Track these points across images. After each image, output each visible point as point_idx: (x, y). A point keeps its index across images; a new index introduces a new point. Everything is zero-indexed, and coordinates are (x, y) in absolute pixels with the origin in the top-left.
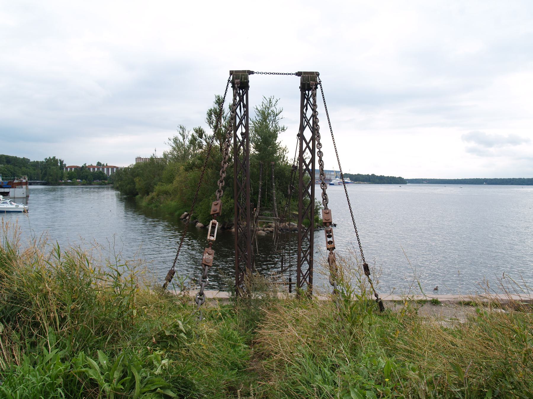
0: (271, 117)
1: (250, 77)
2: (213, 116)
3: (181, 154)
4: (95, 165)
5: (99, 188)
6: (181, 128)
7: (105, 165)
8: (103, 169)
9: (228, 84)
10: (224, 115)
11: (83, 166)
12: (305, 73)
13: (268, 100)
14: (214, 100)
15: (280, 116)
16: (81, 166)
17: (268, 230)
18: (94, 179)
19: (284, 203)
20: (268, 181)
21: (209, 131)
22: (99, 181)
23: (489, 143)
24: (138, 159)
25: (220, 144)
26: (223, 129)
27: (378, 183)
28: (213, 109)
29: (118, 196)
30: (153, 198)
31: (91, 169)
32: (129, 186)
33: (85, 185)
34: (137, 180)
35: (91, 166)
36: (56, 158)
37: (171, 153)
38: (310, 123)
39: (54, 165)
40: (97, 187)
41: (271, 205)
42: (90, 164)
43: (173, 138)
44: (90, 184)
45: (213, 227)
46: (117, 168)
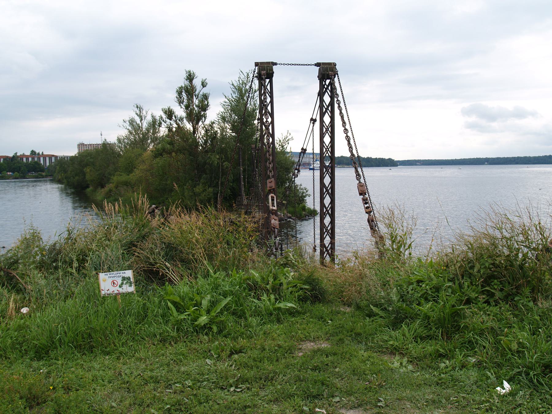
1: (274, 67)
2: (184, 94)
3: (139, 138)
4: (29, 154)
5: (35, 181)
6: (137, 107)
7: (41, 153)
8: (39, 159)
10: (197, 93)
11: (14, 156)
12: (324, 64)
13: (246, 75)
14: (185, 75)
16: (11, 155)
18: (29, 171)
20: (248, 167)
21: (180, 112)
22: (34, 174)
23: (491, 117)
24: (81, 145)
25: (193, 126)
26: (196, 109)
28: (183, 86)
29: (62, 190)
30: (110, 191)
31: (25, 160)
32: (77, 178)
33: (17, 178)
34: (87, 170)
35: (24, 155)
37: (128, 138)
40: (32, 181)
42: (22, 153)
43: (128, 119)
44: (24, 177)
45: (273, 200)
46: (56, 157)
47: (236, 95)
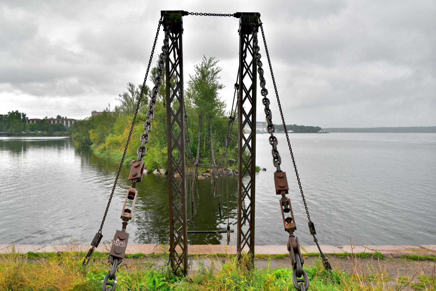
0: (210, 76)
1: (184, 18)
6: (130, 85)
7: (65, 118)
9: (159, 26)
12: (244, 14)
15: (218, 75)
17: (206, 175)
18: (55, 131)
19: (221, 151)
24: (94, 113)
27: (299, 132)
31: (52, 122)
35: (52, 119)
36: (19, 112)
38: (251, 66)
39: (17, 118)
41: (209, 153)
42: (50, 117)
43: (123, 94)
46: (75, 120)
47: (199, 76)
